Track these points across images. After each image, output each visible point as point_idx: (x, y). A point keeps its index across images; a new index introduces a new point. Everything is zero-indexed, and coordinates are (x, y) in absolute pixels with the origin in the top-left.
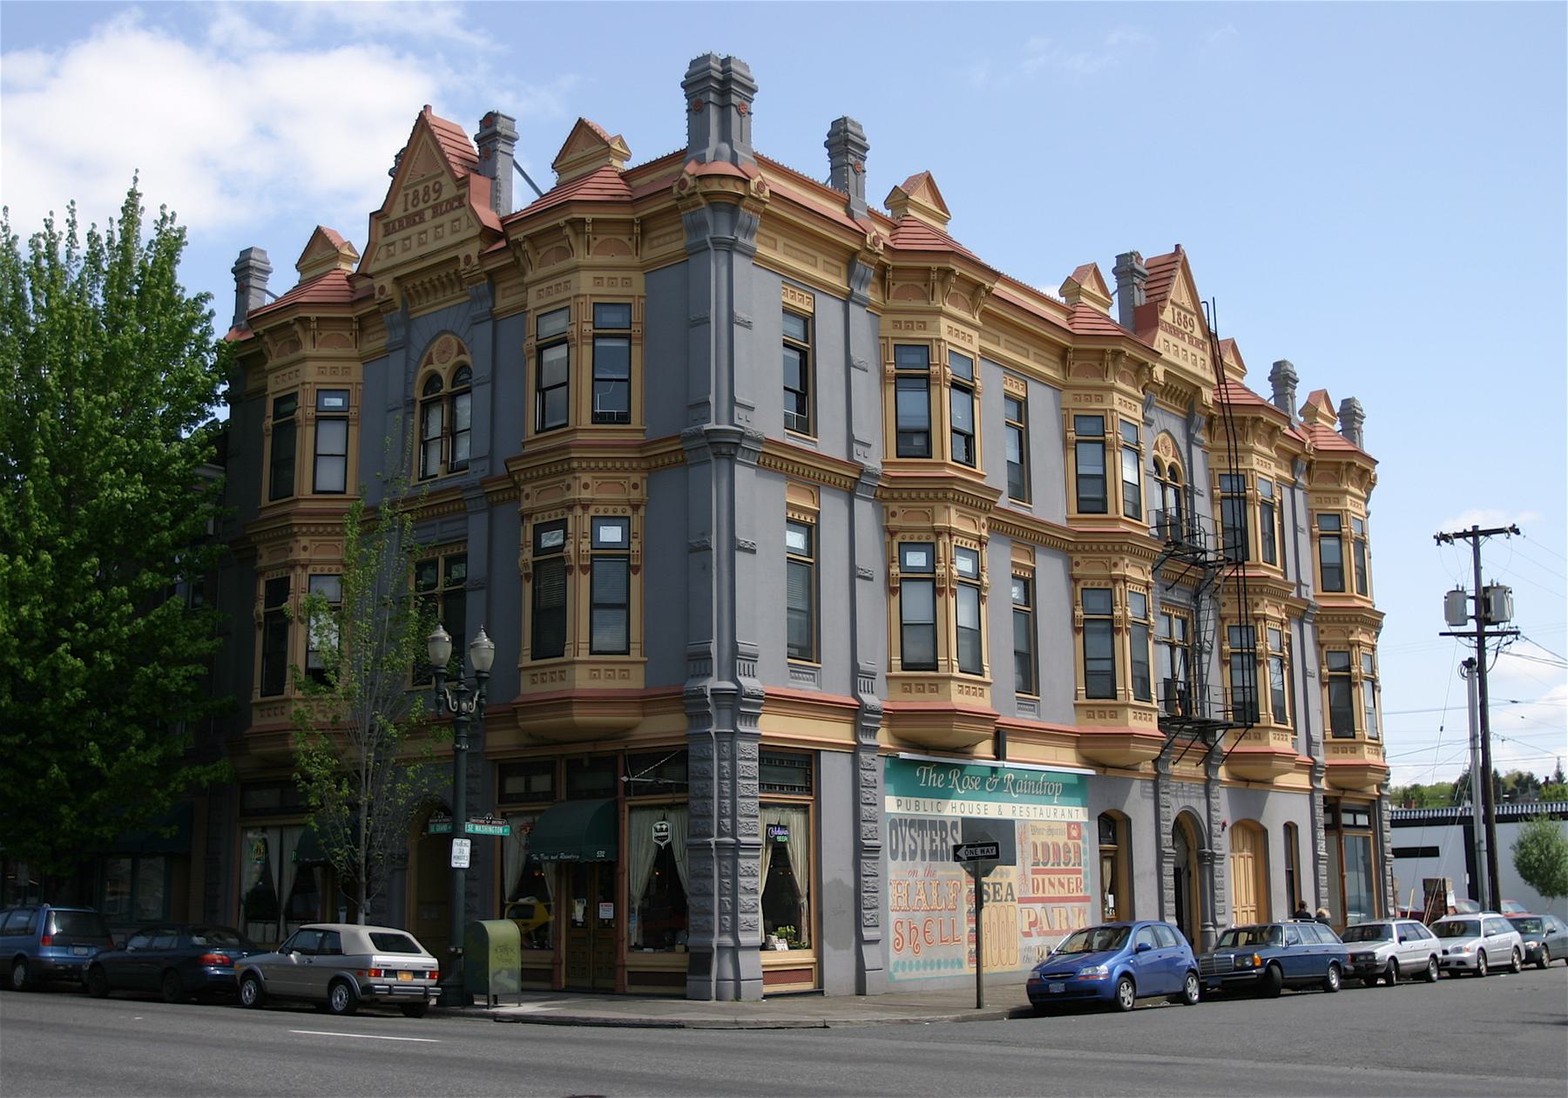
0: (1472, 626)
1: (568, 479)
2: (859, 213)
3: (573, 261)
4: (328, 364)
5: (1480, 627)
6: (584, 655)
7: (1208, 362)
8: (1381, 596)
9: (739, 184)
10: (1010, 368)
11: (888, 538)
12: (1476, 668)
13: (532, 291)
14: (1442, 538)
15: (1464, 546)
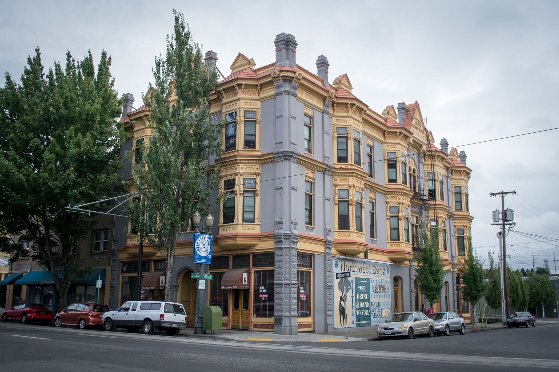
0: (501, 222)
1: (236, 166)
2: (326, 85)
3: (238, 97)
4: (248, 101)
5: (503, 222)
6: (241, 222)
7: (425, 138)
8: (472, 212)
9: (293, 74)
10: (369, 137)
11: (334, 187)
12: (502, 235)
13: (224, 107)
14: (493, 194)
15: (499, 197)
